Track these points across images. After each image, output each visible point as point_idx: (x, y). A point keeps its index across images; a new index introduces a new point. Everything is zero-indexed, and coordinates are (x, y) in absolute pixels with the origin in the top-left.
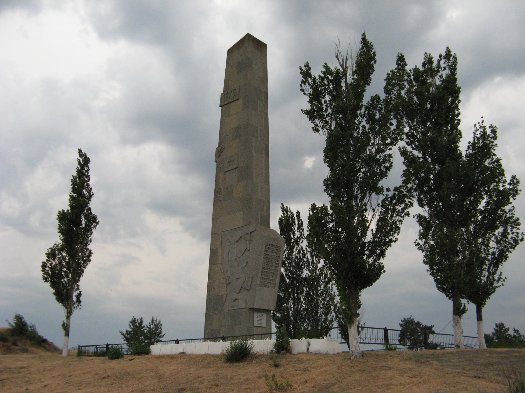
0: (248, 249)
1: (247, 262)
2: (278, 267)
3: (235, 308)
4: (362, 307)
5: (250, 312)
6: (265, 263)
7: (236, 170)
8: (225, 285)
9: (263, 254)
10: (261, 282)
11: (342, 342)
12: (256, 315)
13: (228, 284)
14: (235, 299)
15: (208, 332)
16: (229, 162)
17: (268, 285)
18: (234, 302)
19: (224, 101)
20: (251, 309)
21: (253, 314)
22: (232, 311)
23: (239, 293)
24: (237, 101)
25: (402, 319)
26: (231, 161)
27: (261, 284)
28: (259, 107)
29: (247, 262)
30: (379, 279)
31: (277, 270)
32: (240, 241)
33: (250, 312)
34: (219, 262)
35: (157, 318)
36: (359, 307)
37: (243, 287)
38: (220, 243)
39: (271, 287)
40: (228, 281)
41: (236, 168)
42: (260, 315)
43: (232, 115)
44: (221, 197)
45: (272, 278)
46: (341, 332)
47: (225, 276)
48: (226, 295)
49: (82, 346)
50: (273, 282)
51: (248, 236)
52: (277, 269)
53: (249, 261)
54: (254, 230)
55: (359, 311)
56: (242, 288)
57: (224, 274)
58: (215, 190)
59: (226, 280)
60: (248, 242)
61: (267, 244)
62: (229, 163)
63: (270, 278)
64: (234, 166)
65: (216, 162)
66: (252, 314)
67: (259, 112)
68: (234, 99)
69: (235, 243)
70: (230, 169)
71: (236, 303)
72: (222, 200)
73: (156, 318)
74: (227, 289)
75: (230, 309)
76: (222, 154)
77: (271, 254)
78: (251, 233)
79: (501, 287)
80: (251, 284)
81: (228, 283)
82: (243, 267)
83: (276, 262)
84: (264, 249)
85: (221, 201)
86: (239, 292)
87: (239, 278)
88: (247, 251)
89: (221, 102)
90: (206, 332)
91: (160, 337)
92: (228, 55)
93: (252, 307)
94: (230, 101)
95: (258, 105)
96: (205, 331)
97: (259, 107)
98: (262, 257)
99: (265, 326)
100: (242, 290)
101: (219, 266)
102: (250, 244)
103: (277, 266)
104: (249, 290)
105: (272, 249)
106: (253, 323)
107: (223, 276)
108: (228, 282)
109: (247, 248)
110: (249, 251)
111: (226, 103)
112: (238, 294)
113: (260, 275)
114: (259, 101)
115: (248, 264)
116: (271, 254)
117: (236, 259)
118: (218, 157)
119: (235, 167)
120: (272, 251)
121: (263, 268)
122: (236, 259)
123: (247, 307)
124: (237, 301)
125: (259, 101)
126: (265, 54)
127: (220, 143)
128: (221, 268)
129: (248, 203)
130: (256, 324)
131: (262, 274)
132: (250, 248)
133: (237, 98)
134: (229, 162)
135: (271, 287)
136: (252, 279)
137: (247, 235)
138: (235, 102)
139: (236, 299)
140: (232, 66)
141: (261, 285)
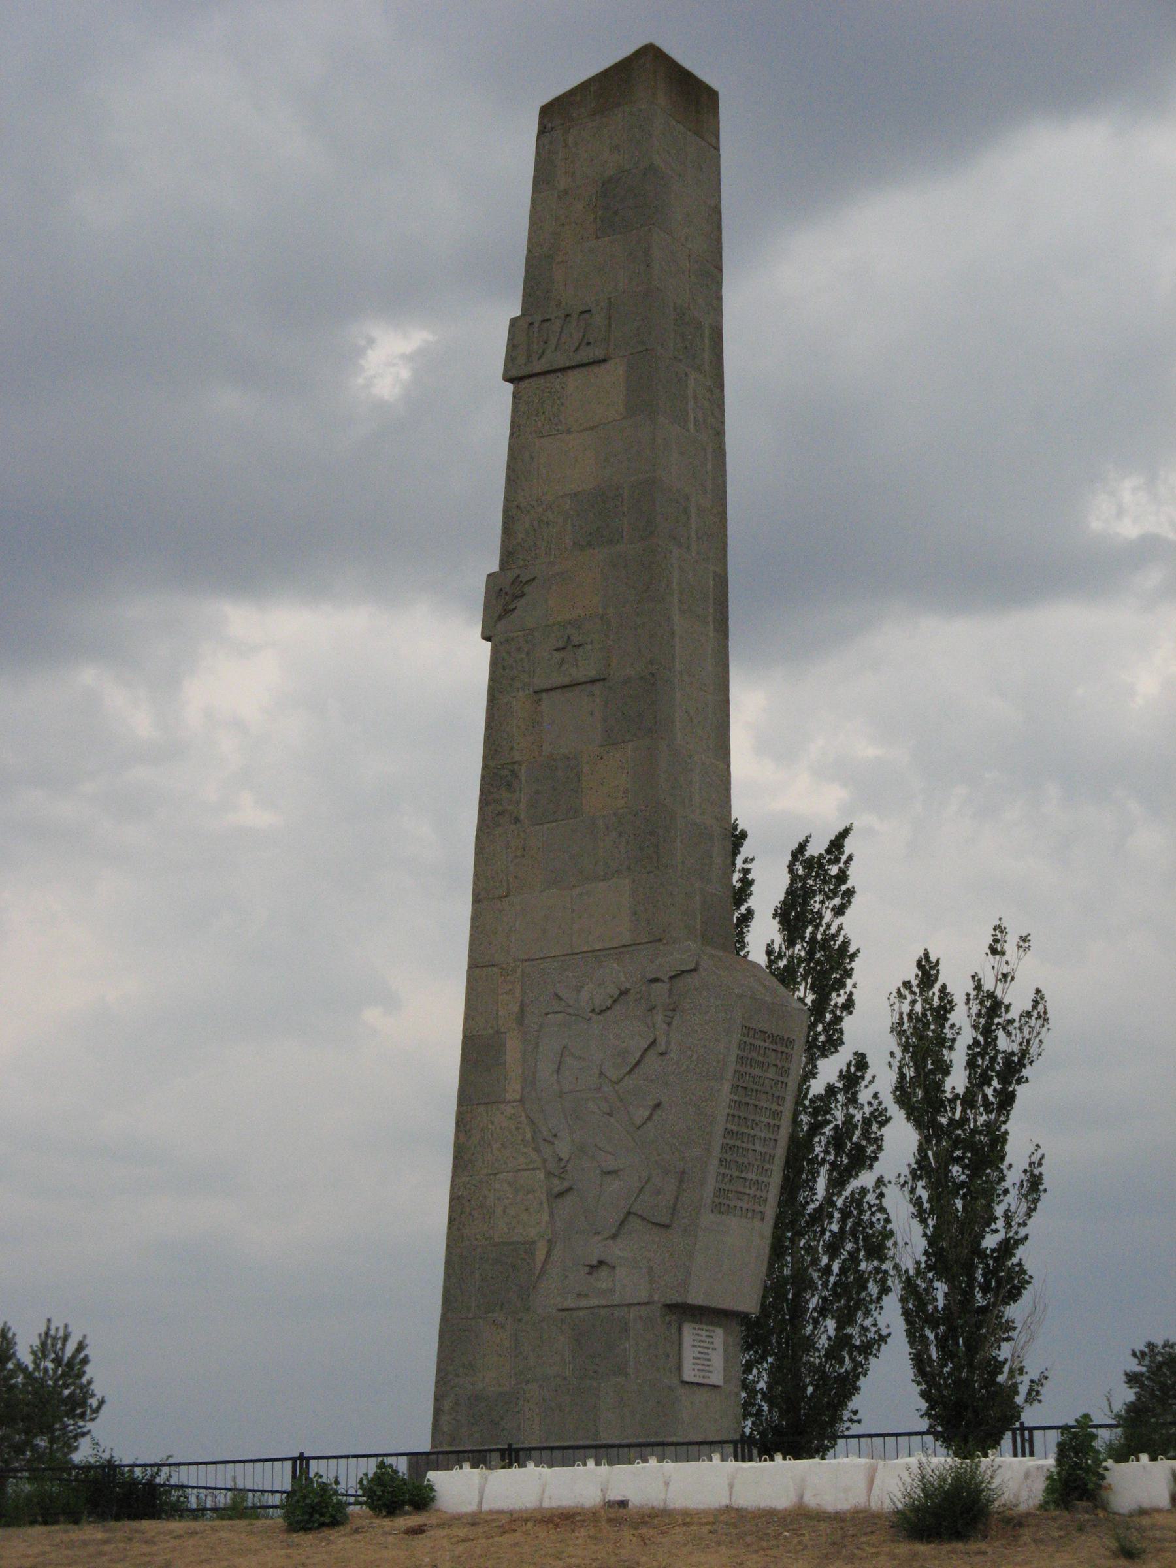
0: (663, 1048)
1: (658, 1105)
2: (778, 1127)
3: (594, 1302)
4: (1027, 1294)
5: (669, 1323)
6: (736, 1113)
7: (597, 689)
8: (544, 1197)
9: (729, 1075)
10: (718, 1192)
11: (394, 1458)
12: (690, 1334)
13: (561, 1194)
14: (595, 1262)
15: (457, 1404)
16: (557, 650)
17: (739, 1204)
18: (590, 1273)
19: (529, 357)
20: (671, 1308)
21: (680, 1330)
22: (581, 1313)
23: (614, 1237)
24: (595, 369)
25: (1140, 1346)
26: (568, 646)
27: (717, 1200)
28: (691, 404)
29: (658, 1105)
30: (908, 1119)
31: (776, 1141)
32: (617, 1007)
33: (669, 1323)
34: (513, 1090)
35: (70, 1329)
36: (1014, 1294)
37: (631, 1211)
38: (515, 1008)
39: (750, 1215)
40: (556, 1181)
41: (593, 682)
42: (704, 1333)
43: (569, 431)
44: (518, 802)
45: (755, 1177)
46: (931, 1408)
47: (544, 1161)
48: (549, 1241)
49: (308, 1459)
50: (758, 1193)
51: (661, 989)
52: (773, 1137)
53: (664, 1099)
54: (692, 966)
55: (1014, 1312)
56: (629, 1213)
57: (537, 1150)
58: (485, 767)
59: (549, 1174)
60: (659, 1018)
61: (748, 1030)
62: (558, 655)
63: (749, 1176)
64: (586, 669)
65: (487, 638)
66: (674, 1327)
67: (691, 426)
68: (585, 355)
69: (595, 1017)
70: (566, 681)
71: (603, 1280)
72: (522, 816)
73: (66, 1326)
74: (552, 1215)
75: (570, 1303)
76: (521, 603)
77: (757, 1071)
78: (671, 978)
79: (1046, 1004)
80: (677, 1198)
81: (556, 1190)
82: (638, 1123)
83: (774, 1107)
84: (735, 1052)
85: (517, 820)
86: (613, 1231)
87: (615, 1172)
88: (651, 1056)
89: (510, 359)
90: (447, 1405)
91: (82, 1416)
92: (542, 131)
93: (677, 1299)
94: (561, 361)
95: (690, 392)
96: (438, 1398)
97: (691, 404)
98: (727, 1087)
99: (720, 1382)
100: (634, 1223)
101: (509, 1110)
102: (669, 1024)
103: (776, 1122)
104: (667, 1227)
105: (762, 1051)
106: (679, 1368)
107: (533, 1155)
108: (557, 1185)
109: (654, 1042)
110: (662, 1054)
111: (538, 367)
112: (610, 1242)
113: (713, 1167)
114: (693, 375)
115: (659, 1112)
116: (757, 1071)
117: (599, 1089)
118: (500, 618)
119: (592, 673)
120: (761, 1059)
121: (728, 1133)
122: (599, 1089)
123: (656, 1298)
124: (604, 1272)
125: (693, 375)
126: (714, 141)
127: (508, 556)
128: (523, 1119)
129: (657, 846)
130: (689, 1375)
131: (721, 1161)
132: (668, 1043)
133: (599, 353)
134: (557, 650)
135: (750, 1215)
136: (681, 1181)
137: (654, 986)
138: (583, 370)
139: (601, 1263)
140: (566, 192)
141: (717, 1208)
